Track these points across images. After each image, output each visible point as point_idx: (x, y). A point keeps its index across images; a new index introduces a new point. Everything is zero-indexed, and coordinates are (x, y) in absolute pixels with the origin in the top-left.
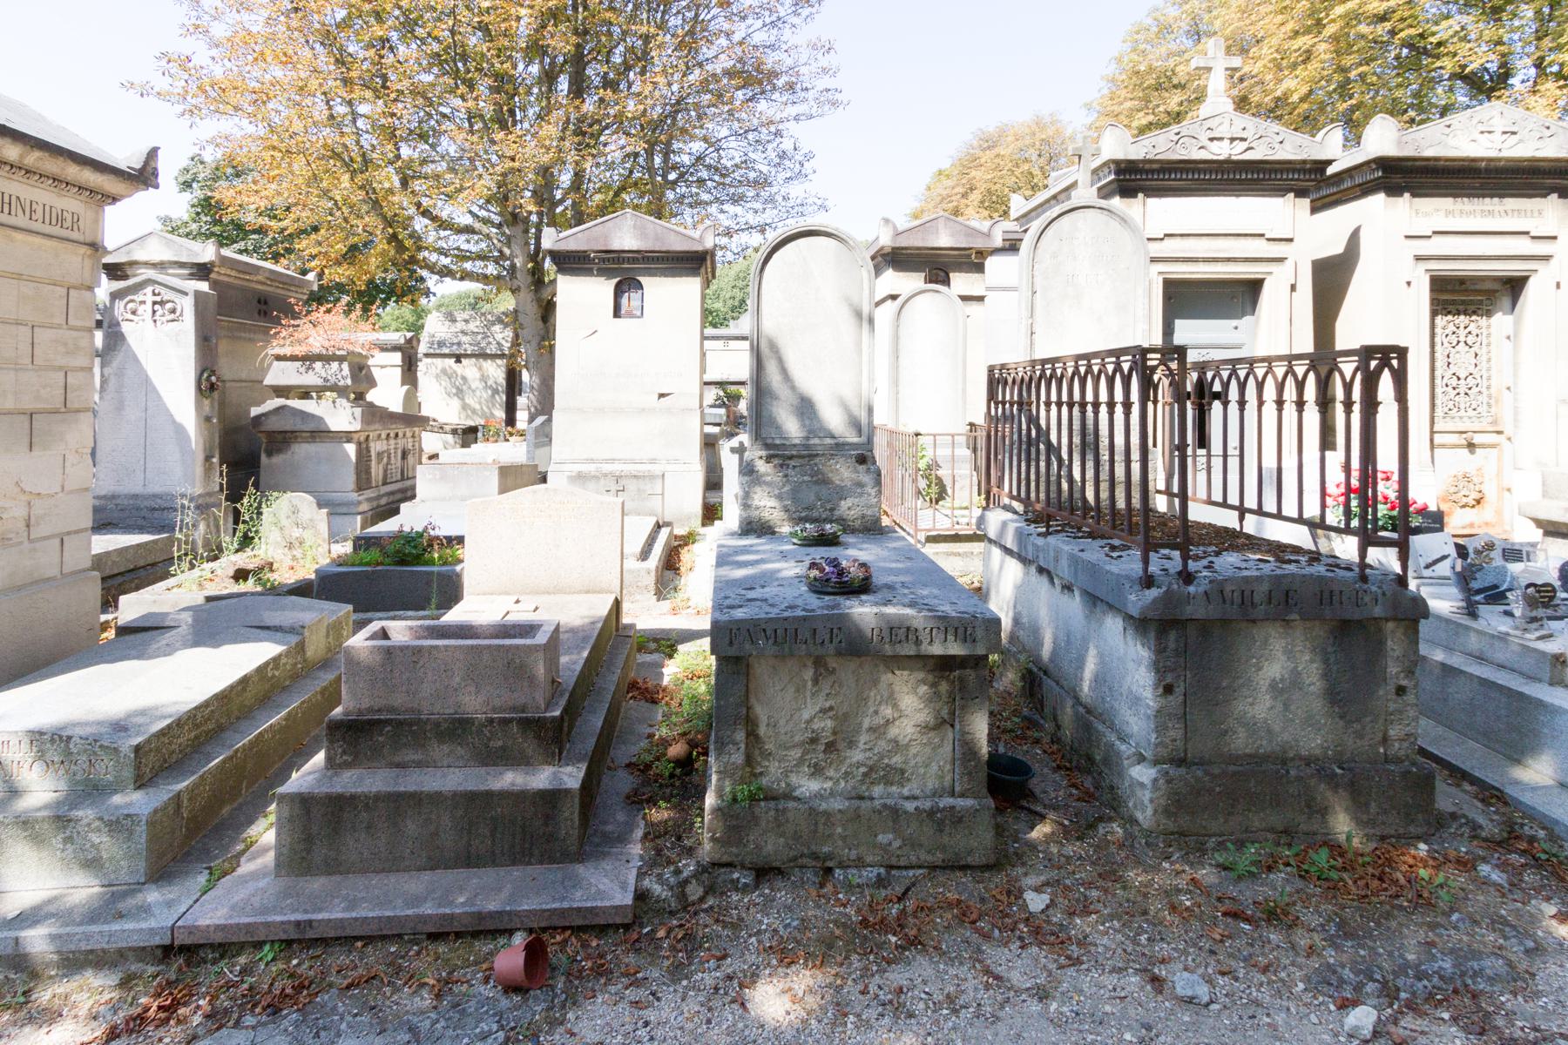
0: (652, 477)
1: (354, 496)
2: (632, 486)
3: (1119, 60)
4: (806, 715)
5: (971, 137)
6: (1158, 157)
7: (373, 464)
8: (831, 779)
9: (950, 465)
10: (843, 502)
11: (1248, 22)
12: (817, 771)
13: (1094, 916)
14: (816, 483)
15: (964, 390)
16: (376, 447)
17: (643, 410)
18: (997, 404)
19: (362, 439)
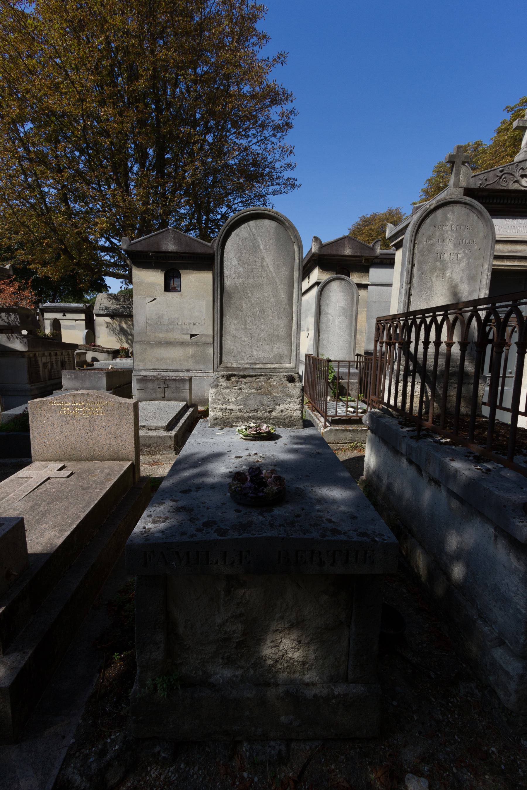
0: (183, 380)
1: (28, 386)
2: (172, 385)
3: (430, 181)
4: (219, 621)
6: (488, 187)
7: (41, 369)
8: (242, 668)
9: (347, 377)
10: (278, 407)
11: (494, 161)
12: (229, 662)
14: (261, 394)
15: (355, 336)
16: (42, 360)
17: (182, 343)
18: (382, 343)
19: (31, 355)
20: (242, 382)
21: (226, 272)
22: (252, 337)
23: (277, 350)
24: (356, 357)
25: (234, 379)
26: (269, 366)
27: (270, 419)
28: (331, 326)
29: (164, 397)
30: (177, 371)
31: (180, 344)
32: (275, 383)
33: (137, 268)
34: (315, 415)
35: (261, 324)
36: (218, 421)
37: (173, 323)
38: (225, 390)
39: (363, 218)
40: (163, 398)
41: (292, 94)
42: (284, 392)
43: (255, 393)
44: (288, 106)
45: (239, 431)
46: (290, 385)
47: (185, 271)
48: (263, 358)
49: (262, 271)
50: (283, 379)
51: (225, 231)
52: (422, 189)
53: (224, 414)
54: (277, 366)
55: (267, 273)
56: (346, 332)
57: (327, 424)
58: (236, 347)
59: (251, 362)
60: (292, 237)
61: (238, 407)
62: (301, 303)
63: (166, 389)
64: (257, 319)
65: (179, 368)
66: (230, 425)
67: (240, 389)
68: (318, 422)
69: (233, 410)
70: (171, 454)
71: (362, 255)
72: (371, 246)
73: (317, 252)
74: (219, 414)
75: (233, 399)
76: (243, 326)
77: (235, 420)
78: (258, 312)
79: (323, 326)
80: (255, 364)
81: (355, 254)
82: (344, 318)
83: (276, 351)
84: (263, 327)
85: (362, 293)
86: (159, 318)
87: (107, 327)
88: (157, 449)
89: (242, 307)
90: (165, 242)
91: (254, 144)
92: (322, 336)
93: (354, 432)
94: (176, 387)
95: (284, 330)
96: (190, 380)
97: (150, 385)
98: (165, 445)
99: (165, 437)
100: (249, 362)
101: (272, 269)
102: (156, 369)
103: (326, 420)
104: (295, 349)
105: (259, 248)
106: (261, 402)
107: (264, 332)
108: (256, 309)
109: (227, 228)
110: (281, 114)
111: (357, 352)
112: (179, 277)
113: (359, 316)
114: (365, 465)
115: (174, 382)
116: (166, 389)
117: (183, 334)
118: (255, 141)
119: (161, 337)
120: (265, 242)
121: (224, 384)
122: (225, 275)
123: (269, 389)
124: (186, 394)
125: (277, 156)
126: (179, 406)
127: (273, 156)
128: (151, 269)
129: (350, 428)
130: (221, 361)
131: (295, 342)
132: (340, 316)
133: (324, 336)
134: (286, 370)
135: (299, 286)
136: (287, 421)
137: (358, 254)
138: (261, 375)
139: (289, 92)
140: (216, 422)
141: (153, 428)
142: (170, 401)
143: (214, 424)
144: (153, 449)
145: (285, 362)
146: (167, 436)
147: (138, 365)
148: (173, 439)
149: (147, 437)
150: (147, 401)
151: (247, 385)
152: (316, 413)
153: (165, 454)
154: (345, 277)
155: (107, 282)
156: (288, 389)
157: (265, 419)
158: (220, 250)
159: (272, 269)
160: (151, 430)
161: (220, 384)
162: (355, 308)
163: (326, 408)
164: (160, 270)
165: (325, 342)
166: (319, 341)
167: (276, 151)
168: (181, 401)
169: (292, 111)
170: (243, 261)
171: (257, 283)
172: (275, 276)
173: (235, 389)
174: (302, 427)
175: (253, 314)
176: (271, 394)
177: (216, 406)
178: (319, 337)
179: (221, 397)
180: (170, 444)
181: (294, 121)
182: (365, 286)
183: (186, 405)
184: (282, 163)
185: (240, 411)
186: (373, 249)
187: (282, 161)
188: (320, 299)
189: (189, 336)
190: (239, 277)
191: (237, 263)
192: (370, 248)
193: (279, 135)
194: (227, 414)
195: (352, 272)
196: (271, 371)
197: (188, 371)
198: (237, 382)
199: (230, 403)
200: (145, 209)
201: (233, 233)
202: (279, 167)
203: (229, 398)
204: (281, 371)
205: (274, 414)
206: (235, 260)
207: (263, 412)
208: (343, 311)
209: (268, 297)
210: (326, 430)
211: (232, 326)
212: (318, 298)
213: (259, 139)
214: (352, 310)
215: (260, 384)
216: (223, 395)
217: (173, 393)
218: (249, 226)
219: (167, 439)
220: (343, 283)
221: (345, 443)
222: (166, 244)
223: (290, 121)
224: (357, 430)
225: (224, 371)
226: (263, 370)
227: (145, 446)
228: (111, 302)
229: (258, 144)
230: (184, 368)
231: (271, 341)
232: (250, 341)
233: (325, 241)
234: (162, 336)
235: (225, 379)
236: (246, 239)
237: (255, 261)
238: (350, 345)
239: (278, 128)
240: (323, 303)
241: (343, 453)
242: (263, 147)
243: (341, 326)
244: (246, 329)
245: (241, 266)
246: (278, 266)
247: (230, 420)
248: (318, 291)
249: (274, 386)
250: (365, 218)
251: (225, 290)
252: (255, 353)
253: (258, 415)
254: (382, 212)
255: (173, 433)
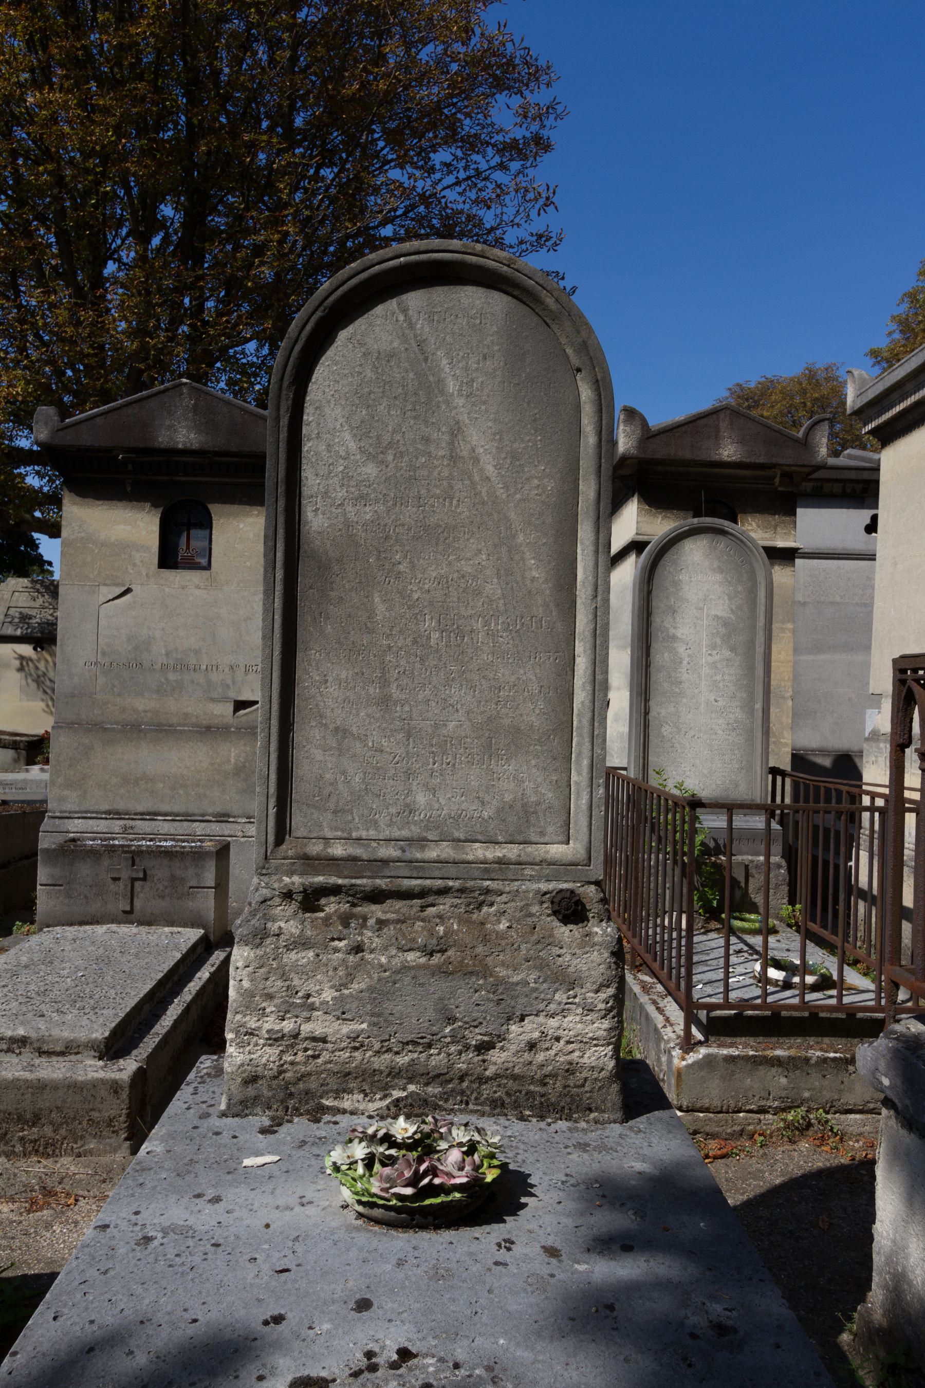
0: (198, 856)
2: (160, 871)
5: (727, 394)
10: (514, 1028)
13: (809, 1191)
14: (443, 972)
15: (766, 711)
17: (208, 728)
20: (365, 919)
21: (311, 480)
22: (409, 735)
23: (512, 786)
24: (770, 776)
25: (332, 906)
26: (479, 851)
27: (482, 1080)
28: (685, 677)
29: (131, 912)
30: (188, 817)
31: (200, 733)
32: (503, 926)
33: (78, 499)
34: (646, 988)
35: (448, 684)
36: (262, 1086)
37: (182, 666)
38: (293, 956)
39: (738, 389)
40: (128, 916)
41: (548, 68)
42: (542, 966)
43: (419, 967)
44: (539, 96)
45: (336, 1168)
46: (564, 932)
47: (227, 508)
48: (457, 819)
49: (451, 478)
50: (535, 909)
51: (309, 327)
52: (893, 317)
53: (288, 1058)
54: (511, 852)
55: (473, 484)
56: (734, 696)
57: (694, 1030)
58: (344, 773)
59: (405, 833)
60: (569, 351)
61: (346, 1029)
62: (607, 601)
63: (138, 884)
64: (432, 662)
65: (193, 808)
66: (311, 1104)
67: (358, 949)
68: (659, 1020)
69: (324, 1040)
70: (115, 1150)
71: (774, 460)
72: (800, 435)
73: (633, 451)
74: (268, 1055)
75: (328, 995)
76: (374, 690)
77: (333, 1083)
78: (435, 636)
79: (659, 680)
80: (421, 842)
81: (752, 459)
82: (727, 653)
83: (507, 790)
84: (455, 693)
85: (781, 575)
86: (136, 648)
87: (21, 669)
88: (63, 1132)
89: (371, 614)
90: (167, 423)
91: (448, 187)
92: (658, 710)
93: (796, 1067)
94: (173, 878)
95: (541, 705)
96: (223, 852)
97: (85, 870)
98: (95, 1115)
99: (96, 1084)
100: (396, 834)
101: (490, 470)
102: (118, 813)
103: (690, 1019)
104: (585, 783)
105: (442, 392)
106: (445, 1008)
107: (461, 715)
108: (429, 624)
109: (319, 314)
110: (520, 111)
111: (771, 764)
112: (207, 524)
113: (774, 648)
114: (878, 1260)
115: (165, 862)
116: (138, 884)
117: (213, 700)
118: (450, 180)
119: (141, 708)
120: (466, 369)
121: (292, 928)
122: (306, 491)
123: (480, 950)
124: (206, 903)
125: (510, 211)
126: (177, 947)
127: (499, 211)
128: (120, 500)
129: (779, 1052)
130: (282, 831)
131: (586, 753)
132: (713, 647)
133: (663, 712)
134: (547, 870)
135: (597, 533)
136: (554, 1089)
137: (761, 460)
138: (443, 892)
139: (542, 63)
140: (251, 1091)
141: (58, 1049)
142: (149, 924)
143: (244, 1103)
144: (48, 1131)
145: (542, 834)
146: (102, 1081)
147: (62, 799)
148: (125, 1095)
149: (28, 1084)
150: (71, 924)
151: (389, 931)
152: (647, 978)
153: (90, 1152)
154: (726, 524)
155: (41, 550)
156: (556, 951)
157: (462, 1079)
158: (288, 396)
159: (490, 470)
160: (49, 1053)
161: (273, 927)
162: (761, 622)
163: (690, 965)
164: (148, 505)
165: (666, 730)
166: (646, 726)
167: (507, 198)
168: (185, 925)
169: (551, 107)
170: (378, 437)
171: (432, 520)
172: (501, 493)
173: (336, 950)
174: (619, 1115)
175: (415, 642)
176: (486, 972)
177: (253, 1024)
178: (647, 713)
179: (276, 985)
180: (112, 1113)
181: (554, 132)
182: (787, 556)
183: (204, 939)
184: (521, 233)
185: (356, 1043)
186: (806, 444)
187: (525, 225)
188: (649, 592)
189: (230, 707)
190: (362, 498)
191: (352, 445)
192: (797, 441)
193: (515, 166)
194: (300, 1057)
195: (745, 513)
196: (487, 874)
197: (223, 818)
198: (345, 920)
199: (312, 1008)
200: (135, 344)
201: (343, 335)
202: (514, 241)
203: (312, 987)
204: (528, 872)
205: (498, 1057)
206: (347, 436)
207: (453, 1049)
208: (723, 630)
209: (475, 578)
210: (692, 1058)
211: (332, 690)
212: (641, 590)
213: (462, 175)
214: (753, 627)
215: (441, 929)
216: (284, 977)
217: (162, 897)
218: (405, 311)
219: (103, 1093)
220: (722, 543)
221: (762, 1111)
222: (170, 427)
223: (545, 133)
224: (807, 1060)
225: (291, 874)
226: (452, 870)
227: (21, 1119)
228: (40, 601)
229: (459, 189)
230: (210, 811)
231: (489, 750)
232: (401, 751)
233: (657, 419)
234: (143, 704)
235: (294, 906)
236: (391, 356)
237: (427, 440)
238: (750, 740)
239: (513, 149)
240: (658, 604)
241: (757, 1151)
242: (473, 197)
243: (719, 678)
244: (385, 702)
245: (371, 457)
246: (515, 456)
247: (313, 1084)
248: (643, 569)
249: (500, 936)
250: (742, 389)
251: (304, 547)
252: (421, 799)
253: (433, 1062)
254: (792, 375)
255: (129, 1066)
